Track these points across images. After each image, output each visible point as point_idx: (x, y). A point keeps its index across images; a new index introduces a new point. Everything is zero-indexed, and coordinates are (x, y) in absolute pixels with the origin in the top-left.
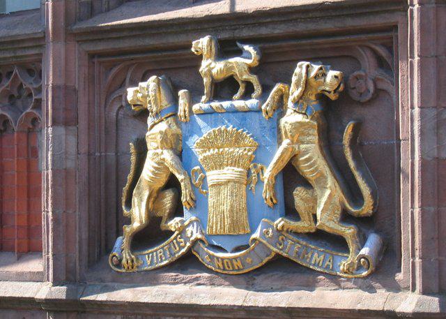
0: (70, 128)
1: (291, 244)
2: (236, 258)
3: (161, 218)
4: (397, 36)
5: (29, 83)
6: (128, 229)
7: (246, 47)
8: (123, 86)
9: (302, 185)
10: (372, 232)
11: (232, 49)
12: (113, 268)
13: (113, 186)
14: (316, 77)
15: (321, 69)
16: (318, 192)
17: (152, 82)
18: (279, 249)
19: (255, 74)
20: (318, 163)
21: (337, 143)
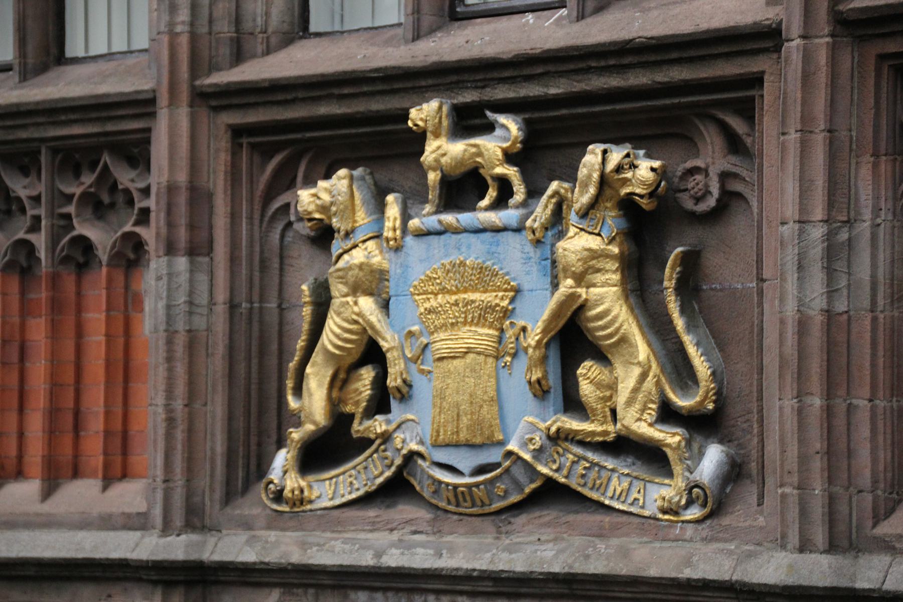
0: (200, 259)
1: (573, 462)
2: (477, 485)
3: (351, 417)
4: (762, 96)
5: (125, 177)
6: (296, 435)
7: (502, 119)
8: (291, 185)
9: (593, 358)
10: (713, 443)
11: (477, 121)
12: (268, 503)
13: (273, 361)
14: (619, 169)
15: (628, 155)
16: (619, 370)
17: (341, 180)
18: (551, 469)
19: (515, 165)
20: (620, 320)
21: (656, 287)
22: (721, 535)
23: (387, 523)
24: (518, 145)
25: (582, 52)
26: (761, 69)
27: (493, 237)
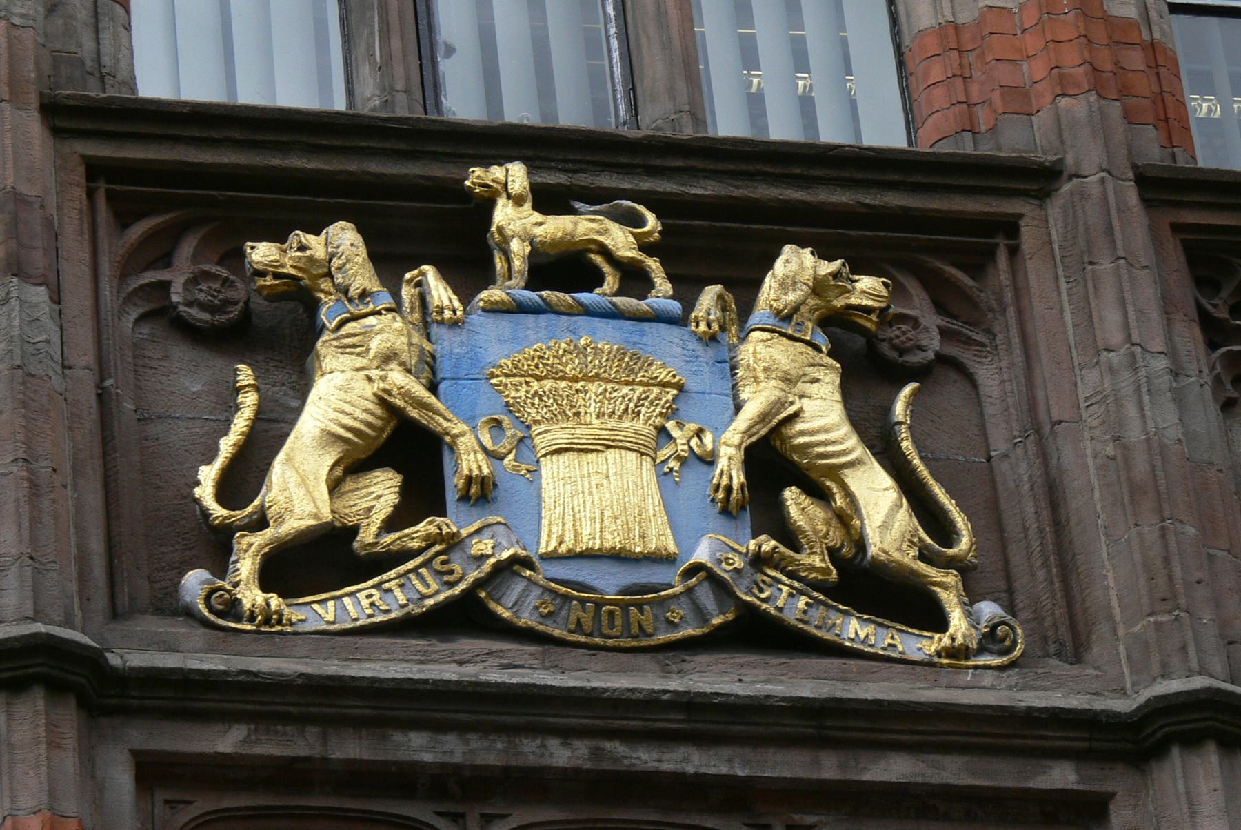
22: (1038, 683)
23: (453, 653)
24: (657, 234)
25: (757, 149)
26: (1018, 212)
27: (633, 325)
